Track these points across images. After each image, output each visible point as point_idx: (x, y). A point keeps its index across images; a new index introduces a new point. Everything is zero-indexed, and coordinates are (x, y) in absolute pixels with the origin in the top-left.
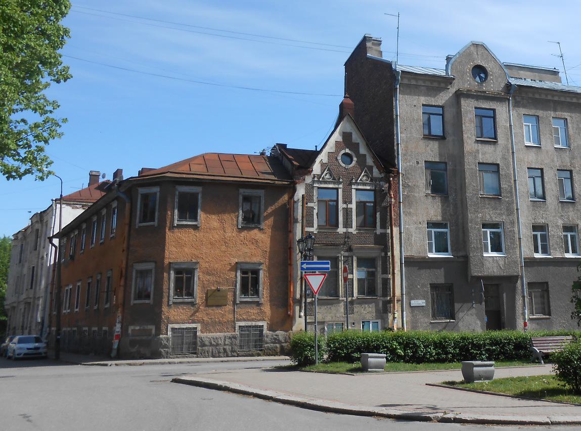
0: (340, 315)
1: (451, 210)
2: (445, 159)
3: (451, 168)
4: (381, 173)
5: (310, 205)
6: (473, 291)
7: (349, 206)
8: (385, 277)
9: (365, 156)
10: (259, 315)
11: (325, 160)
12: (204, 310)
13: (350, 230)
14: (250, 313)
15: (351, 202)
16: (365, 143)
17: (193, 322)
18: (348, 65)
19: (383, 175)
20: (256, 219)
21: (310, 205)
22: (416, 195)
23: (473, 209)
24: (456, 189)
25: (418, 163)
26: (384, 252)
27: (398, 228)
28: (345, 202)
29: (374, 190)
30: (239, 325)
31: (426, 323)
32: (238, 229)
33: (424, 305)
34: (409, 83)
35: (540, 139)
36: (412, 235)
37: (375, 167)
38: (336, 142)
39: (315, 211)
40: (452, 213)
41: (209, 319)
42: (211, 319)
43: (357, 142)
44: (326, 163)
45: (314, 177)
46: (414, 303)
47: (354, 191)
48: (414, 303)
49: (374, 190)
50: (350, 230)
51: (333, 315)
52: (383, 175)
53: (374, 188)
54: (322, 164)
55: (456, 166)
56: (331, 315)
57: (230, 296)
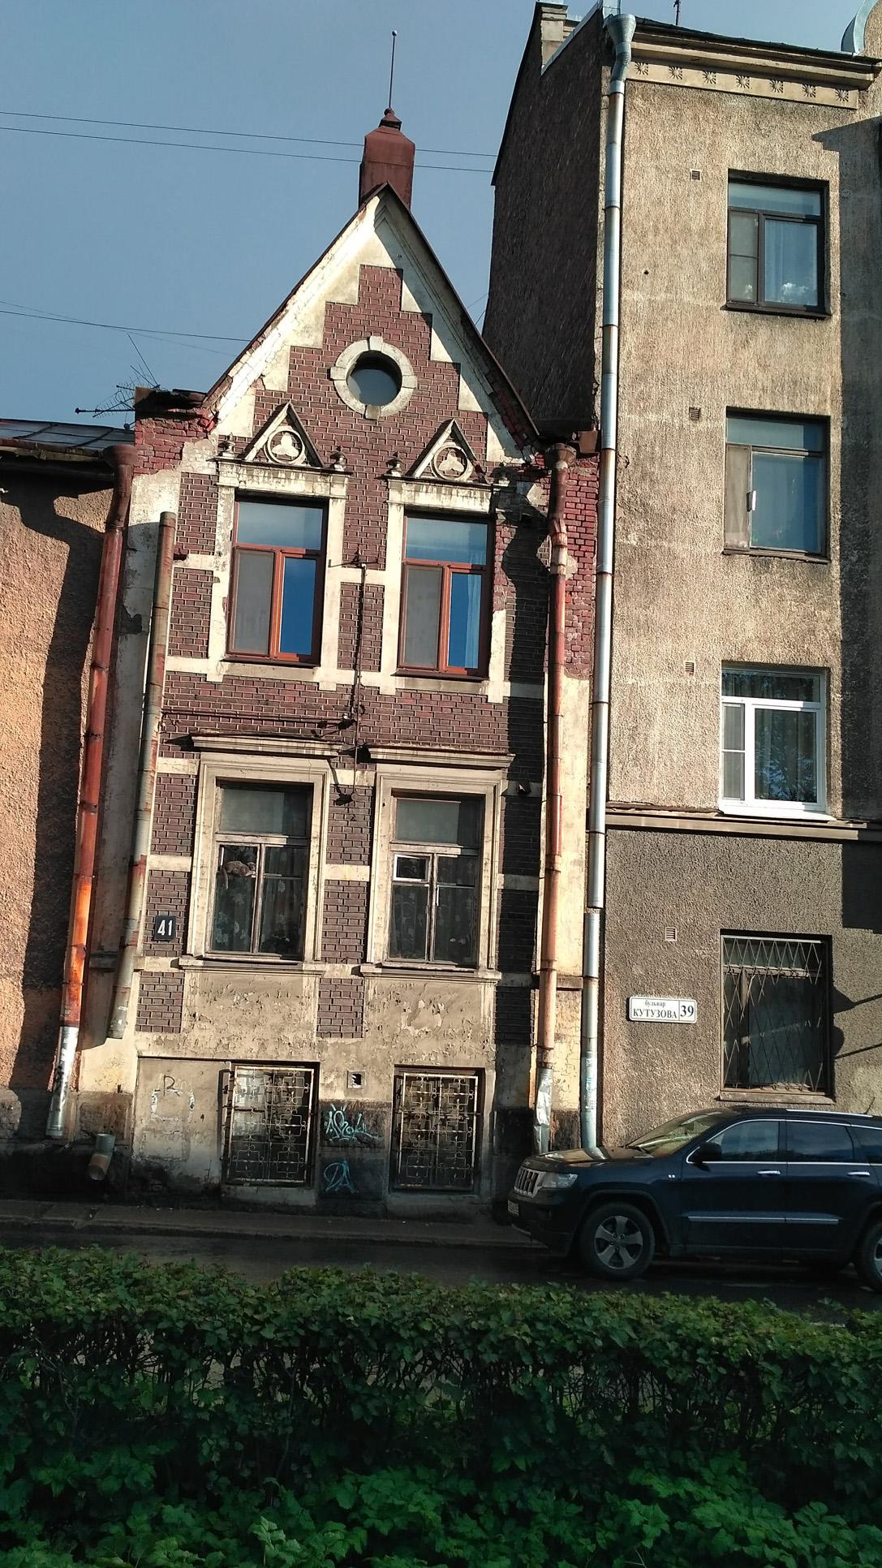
7: (373, 577)
11: (278, 380)
13: (368, 678)
15: (379, 563)
22: (678, 548)
33: (691, 1018)
39: (220, 591)
45: (224, 445)
46: (643, 1007)
47: (396, 516)
48: (643, 1007)
50: (368, 678)
55: (869, 436)
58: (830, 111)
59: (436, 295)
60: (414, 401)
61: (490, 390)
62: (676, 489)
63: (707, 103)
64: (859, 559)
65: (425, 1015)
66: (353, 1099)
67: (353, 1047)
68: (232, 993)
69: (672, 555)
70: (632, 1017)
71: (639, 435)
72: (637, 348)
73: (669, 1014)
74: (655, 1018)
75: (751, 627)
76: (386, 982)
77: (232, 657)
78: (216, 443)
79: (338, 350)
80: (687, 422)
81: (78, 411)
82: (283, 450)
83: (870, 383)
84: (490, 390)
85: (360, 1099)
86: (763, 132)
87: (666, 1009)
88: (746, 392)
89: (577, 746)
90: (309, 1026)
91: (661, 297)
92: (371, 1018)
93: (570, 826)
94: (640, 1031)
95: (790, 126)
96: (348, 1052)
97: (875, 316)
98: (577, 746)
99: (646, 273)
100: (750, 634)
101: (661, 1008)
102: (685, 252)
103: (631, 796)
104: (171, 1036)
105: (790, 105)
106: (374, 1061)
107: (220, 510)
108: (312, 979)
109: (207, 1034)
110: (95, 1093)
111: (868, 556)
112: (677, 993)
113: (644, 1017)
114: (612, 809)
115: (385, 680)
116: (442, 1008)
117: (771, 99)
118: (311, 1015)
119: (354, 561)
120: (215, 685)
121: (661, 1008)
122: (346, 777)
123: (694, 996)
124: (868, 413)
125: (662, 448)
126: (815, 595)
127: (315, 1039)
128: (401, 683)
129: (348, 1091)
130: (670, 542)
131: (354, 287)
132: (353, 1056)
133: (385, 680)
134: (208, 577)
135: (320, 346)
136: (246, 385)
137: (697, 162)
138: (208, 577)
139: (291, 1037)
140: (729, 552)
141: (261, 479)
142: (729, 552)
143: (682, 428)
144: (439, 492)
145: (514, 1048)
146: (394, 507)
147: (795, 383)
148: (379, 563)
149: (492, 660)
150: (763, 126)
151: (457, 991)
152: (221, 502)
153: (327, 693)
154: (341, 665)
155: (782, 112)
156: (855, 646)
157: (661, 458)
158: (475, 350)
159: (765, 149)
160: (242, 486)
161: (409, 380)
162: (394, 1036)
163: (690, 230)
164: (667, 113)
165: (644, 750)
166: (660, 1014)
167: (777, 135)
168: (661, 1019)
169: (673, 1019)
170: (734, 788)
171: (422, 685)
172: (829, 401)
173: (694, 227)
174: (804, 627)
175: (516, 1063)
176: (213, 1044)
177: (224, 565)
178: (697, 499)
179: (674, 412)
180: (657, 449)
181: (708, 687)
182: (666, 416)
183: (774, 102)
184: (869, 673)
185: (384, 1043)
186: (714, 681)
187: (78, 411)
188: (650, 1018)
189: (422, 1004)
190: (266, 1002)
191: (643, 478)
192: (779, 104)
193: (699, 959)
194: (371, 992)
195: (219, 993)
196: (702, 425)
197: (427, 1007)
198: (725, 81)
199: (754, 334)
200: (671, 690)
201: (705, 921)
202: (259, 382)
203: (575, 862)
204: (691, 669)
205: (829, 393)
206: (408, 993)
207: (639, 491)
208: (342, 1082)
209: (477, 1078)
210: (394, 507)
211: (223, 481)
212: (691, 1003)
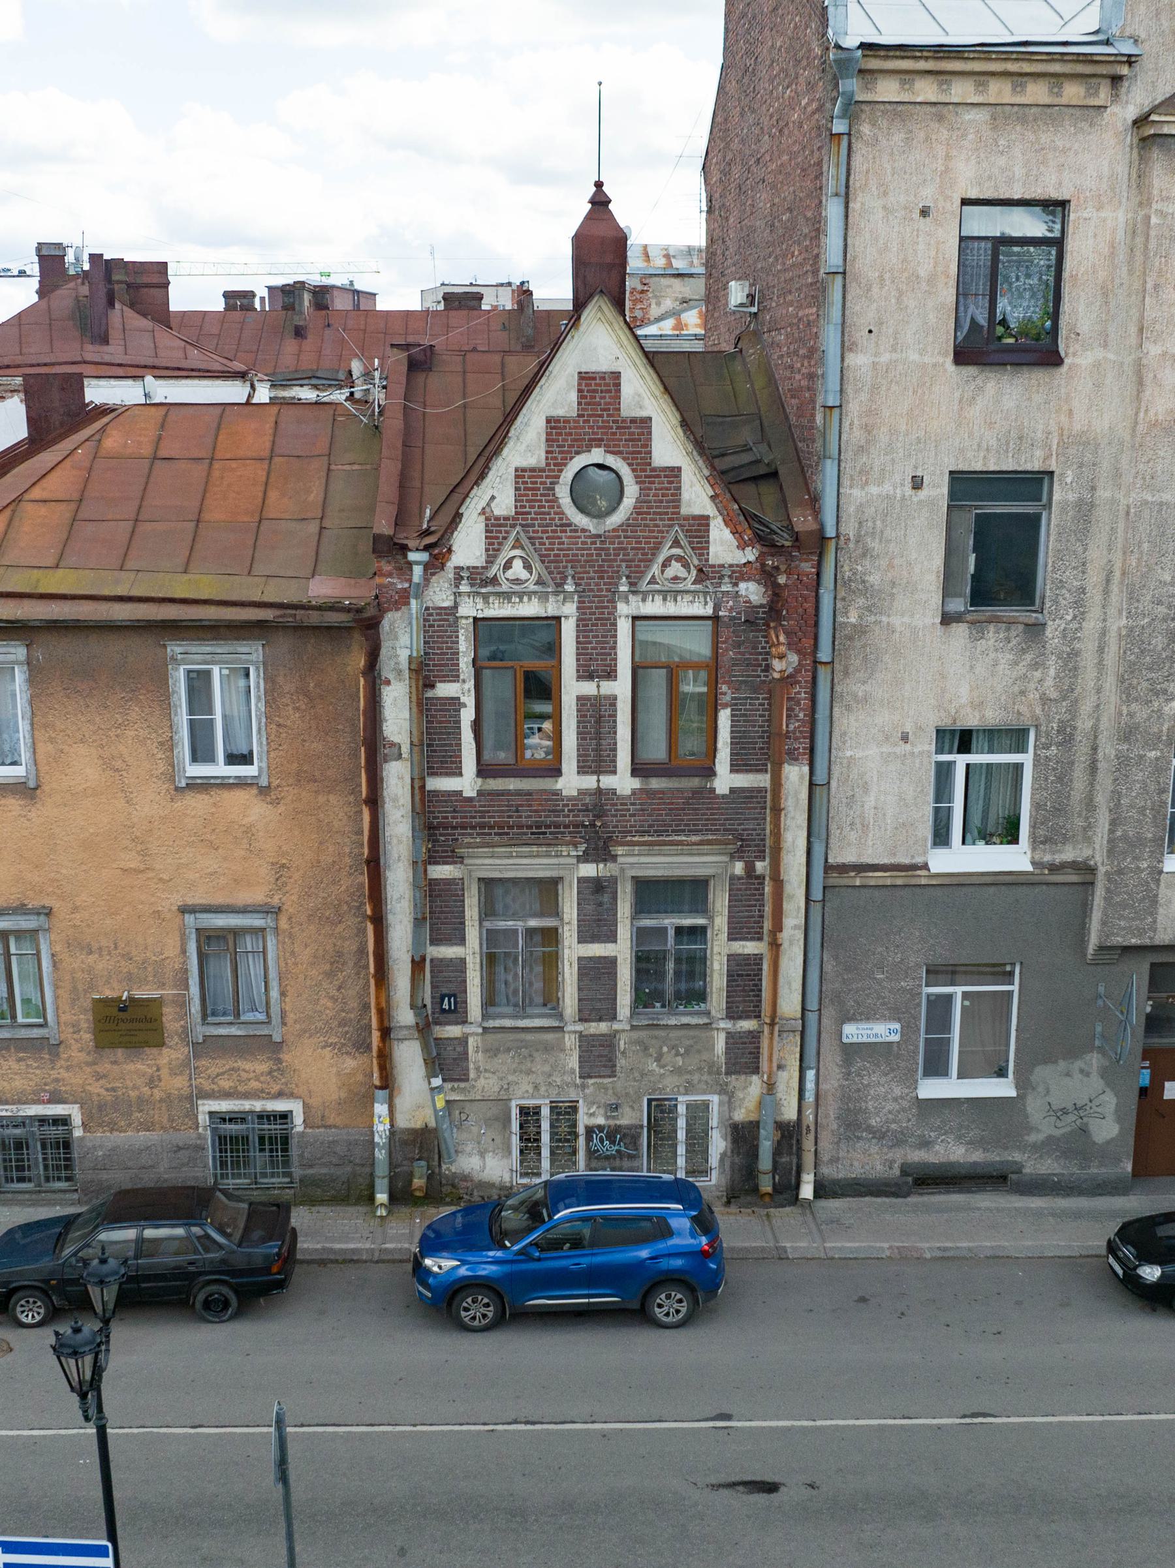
0: (567, 1078)
1: (1049, 682)
2: (1047, 457)
3: (1072, 497)
4: (742, 546)
5: (445, 690)
6: (1101, 989)
7: (607, 688)
8: (740, 951)
9: (674, 473)
10: (275, 1079)
11: (505, 505)
12: (88, 1064)
13: (607, 781)
14: (243, 1074)
15: (610, 674)
16: (674, 418)
17: (56, 1099)
18: (580, 241)
19: (751, 554)
20: (274, 1128)
21: (445, 690)
22: (896, 621)
23: (1145, 685)
24: (1083, 590)
25: (917, 483)
26: (740, 858)
27: (806, 769)
28: (586, 674)
29: (511, 1188)
30: (207, 1109)
31: (895, 1100)
32: (177, 789)
33: (896, 1038)
34: (905, 97)
35: (972, 973)
36: (866, 789)
37: (720, 519)
38: (548, 421)
39: (467, 715)
40: (1054, 695)
41: (107, 1090)
42: (114, 1089)
43: (644, 414)
44: (506, 519)
45: (458, 579)
46: (853, 1032)
47: (624, 628)
48: (853, 1032)
49: (715, 618)
50: (607, 781)
51: (540, 1080)
52: (751, 554)
53: (710, 606)
54: (495, 529)
55: (1093, 488)
56: (532, 1078)
57: (170, 1020)
58: (1078, 112)
59: (656, 397)
60: (637, 510)
61: (711, 493)
62: (896, 562)
63: (940, 118)
64: (1075, 617)
65: (667, 1059)
66: (612, 1122)
67: (610, 1086)
68: (509, 1050)
69: (890, 629)
70: (845, 1040)
71: (860, 508)
72: (860, 416)
73: (876, 1035)
74: (865, 1040)
75: (964, 693)
76: (635, 1035)
77: (484, 771)
78: (451, 576)
79: (561, 466)
80: (908, 490)
81: (600, 84)
82: (514, 573)
83: (1098, 431)
84: (711, 493)
85: (618, 1122)
86: (1001, 148)
87: (874, 1032)
88: (970, 454)
89: (798, 827)
90: (573, 1071)
91: (885, 358)
92: (621, 1062)
93: (791, 897)
94: (851, 1052)
95: (1032, 137)
96: (606, 1089)
97: (1111, 356)
98: (798, 827)
99: (870, 331)
100: (964, 701)
101: (869, 1032)
102: (912, 304)
103: (848, 856)
104: (462, 1085)
105: (1034, 110)
106: (627, 1094)
107: (462, 638)
108: (573, 1036)
109: (491, 1082)
110: (408, 1130)
111: (1083, 613)
112: (884, 1018)
113: (855, 1040)
114: (828, 868)
115: (623, 782)
116: (682, 1051)
117: (1012, 105)
118: (573, 1062)
119: (586, 674)
120: (470, 799)
121: (869, 1032)
122: (589, 870)
123: (899, 1020)
124: (1094, 465)
125: (883, 521)
126: (1029, 657)
127: (578, 1081)
128: (636, 783)
129: (607, 1118)
130: (889, 616)
131: (573, 396)
132: (610, 1092)
133: (623, 782)
134: (455, 703)
135: (543, 464)
136: (475, 514)
137: (927, 195)
138: (455, 703)
139: (558, 1080)
140: (947, 619)
141: (496, 605)
142: (947, 619)
143: (903, 498)
144: (665, 599)
145: (743, 1077)
146: (623, 619)
147: (1021, 438)
148: (610, 674)
149: (718, 756)
150: (1002, 142)
151: (694, 1037)
152: (462, 631)
153: (570, 799)
154: (582, 770)
155: (1023, 121)
156: (1064, 704)
157: (882, 532)
158: (695, 453)
159: (1003, 170)
160: (480, 615)
161: (632, 491)
162: (642, 1075)
163: (918, 277)
164: (898, 137)
165: (862, 816)
166: (868, 1036)
167: (1017, 151)
168: (869, 1040)
169: (879, 1040)
170: (941, 837)
171: (655, 783)
172: (1054, 456)
173: (922, 273)
174: (1016, 689)
175: (745, 1088)
176: (496, 1089)
177: (469, 691)
178: (917, 570)
179: (896, 485)
180: (878, 523)
181: (921, 753)
182: (887, 488)
183: (1016, 108)
184: (1075, 728)
185: (635, 1080)
186: (926, 747)
187: (600, 84)
188: (860, 1040)
189: (665, 1049)
190: (536, 1054)
191: (864, 555)
192: (1021, 111)
193: (904, 990)
194: (622, 1043)
195: (498, 1050)
196: (923, 494)
197: (669, 1051)
198: (961, 90)
199: (980, 389)
200: (886, 759)
201: (913, 960)
202: (487, 510)
203: (796, 927)
204: (905, 738)
205: (1055, 447)
206: (654, 1042)
207: (859, 568)
208: (602, 1111)
209: (715, 1099)
210: (623, 619)
211: (463, 611)
212: (897, 1026)
